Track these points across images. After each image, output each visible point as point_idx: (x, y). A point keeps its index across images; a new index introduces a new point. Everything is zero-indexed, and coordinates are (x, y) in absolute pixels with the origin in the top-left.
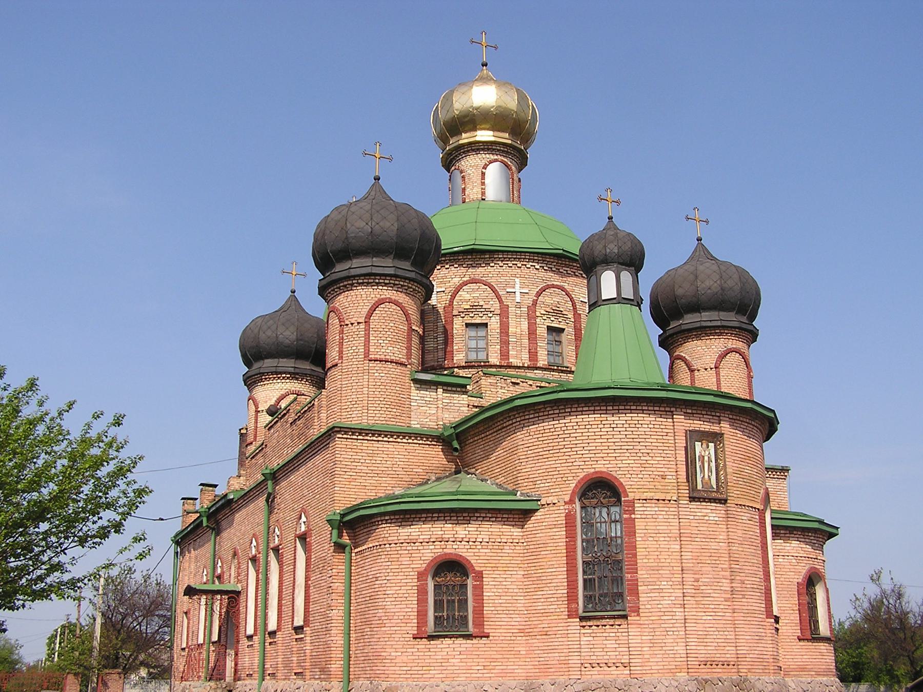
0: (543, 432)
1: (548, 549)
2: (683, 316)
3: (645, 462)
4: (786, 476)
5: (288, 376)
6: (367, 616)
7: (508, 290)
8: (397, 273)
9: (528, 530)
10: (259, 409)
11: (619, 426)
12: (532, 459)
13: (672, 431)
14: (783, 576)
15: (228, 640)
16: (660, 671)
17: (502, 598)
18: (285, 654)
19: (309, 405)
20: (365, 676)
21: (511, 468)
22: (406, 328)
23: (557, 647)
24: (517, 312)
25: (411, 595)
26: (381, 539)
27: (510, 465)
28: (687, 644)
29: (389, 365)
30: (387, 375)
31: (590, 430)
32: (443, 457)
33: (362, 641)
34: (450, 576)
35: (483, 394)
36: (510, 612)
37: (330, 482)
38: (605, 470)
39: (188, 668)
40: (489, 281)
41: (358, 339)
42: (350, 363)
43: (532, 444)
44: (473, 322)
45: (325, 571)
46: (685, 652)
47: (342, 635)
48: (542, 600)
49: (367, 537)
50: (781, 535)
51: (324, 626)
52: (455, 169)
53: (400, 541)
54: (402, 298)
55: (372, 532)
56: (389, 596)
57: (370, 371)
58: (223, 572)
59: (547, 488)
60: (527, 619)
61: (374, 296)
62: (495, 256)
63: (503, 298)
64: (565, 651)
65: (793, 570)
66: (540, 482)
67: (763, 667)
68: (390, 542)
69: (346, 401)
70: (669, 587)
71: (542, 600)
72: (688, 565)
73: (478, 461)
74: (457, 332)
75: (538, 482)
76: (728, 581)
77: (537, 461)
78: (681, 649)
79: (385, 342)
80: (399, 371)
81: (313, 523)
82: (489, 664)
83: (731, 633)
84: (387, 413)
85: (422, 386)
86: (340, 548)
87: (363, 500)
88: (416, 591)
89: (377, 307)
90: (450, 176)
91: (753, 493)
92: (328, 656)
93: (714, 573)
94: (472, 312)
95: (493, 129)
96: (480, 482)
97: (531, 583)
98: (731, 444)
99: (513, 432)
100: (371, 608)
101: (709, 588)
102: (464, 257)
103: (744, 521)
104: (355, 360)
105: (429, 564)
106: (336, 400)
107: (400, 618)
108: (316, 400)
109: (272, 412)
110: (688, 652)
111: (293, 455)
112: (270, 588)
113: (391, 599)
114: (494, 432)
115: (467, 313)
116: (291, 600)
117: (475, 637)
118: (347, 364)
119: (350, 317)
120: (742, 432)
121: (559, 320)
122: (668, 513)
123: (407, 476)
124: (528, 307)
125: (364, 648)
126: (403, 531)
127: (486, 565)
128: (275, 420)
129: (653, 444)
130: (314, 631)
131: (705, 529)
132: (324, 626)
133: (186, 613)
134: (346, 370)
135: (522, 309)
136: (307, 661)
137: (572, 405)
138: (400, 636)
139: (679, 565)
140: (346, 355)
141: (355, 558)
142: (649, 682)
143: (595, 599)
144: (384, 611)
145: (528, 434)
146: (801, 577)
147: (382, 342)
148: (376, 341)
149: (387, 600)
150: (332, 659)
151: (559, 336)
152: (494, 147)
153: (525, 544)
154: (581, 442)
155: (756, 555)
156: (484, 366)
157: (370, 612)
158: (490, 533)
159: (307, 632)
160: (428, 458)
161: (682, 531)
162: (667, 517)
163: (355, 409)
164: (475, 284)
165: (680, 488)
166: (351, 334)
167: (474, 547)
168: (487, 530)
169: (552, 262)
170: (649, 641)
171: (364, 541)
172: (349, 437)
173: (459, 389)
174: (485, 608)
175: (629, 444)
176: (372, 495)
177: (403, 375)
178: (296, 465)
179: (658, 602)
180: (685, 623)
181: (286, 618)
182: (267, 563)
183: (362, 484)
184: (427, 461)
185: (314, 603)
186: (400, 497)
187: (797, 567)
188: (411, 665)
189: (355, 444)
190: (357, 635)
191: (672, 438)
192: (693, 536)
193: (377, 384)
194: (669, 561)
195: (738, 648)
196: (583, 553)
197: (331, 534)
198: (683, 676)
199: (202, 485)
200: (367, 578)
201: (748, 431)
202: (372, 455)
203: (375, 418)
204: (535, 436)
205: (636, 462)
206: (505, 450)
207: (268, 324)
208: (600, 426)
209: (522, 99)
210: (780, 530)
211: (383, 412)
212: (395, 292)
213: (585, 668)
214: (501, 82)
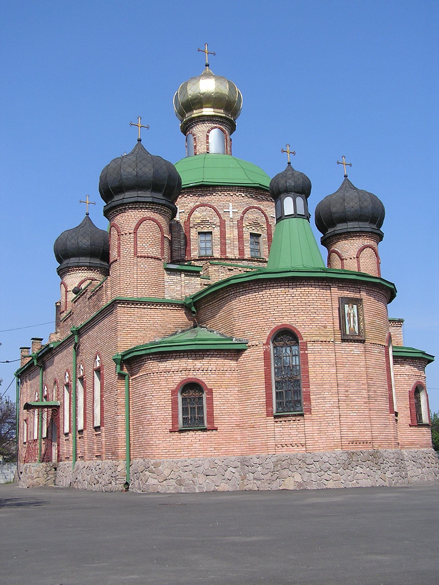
0: (248, 300)
3: (313, 318)
4: (401, 325)
6: (140, 419)
7: (225, 210)
8: (153, 201)
9: (240, 362)
10: (68, 290)
12: (242, 317)
16: (325, 448)
17: (225, 405)
19: (100, 287)
22: (160, 236)
23: (260, 435)
25: (167, 405)
26: (148, 370)
27: (228, 321)
28: (341, 431)
30: (149, 266)
31: (278, 298)
32: (186, 317)
33: (138, 434)
34: (191, 392)
36: (230, 414)
38: (288, 323)
41: (129, 243)
42: (125, 259)
43: (242, 308)
44: (203, 231)
45: (113, 391)
47: (125, 431)
49: (139, 369)
50: (399, 362)
51: (113, 426)
52: (190, 133)
53: (160, 371)
54: (157, 216)
55: (142, 366)
56: (154, 406)
57: (138, 264)
58: (48, 394)
59: (252, 335)
60: (241, 418)
62: (216, 189)
65: (407, 383)
66: (247, 332)
67: (388, 444)
68: (154, 372)
69: (123, 283)
72: (341, 382)
75: (246, 332)
76: (366, 391)
77: (245, 319)
78: (337, 434)
79: (147, 245)
80: (156, 263)
82: (218, 447)
83: (368, 423)
84: (149, 290)
86: (122, 376)
88: (171, 402)
89: (142, 223)
92: (116, 444)
93: (357, 386)
94: (202, 225)
95: (213, 107)
96: (209, 333)
97: (243, 395)
99: (230, 301)
100: (143, 414)
101: (354, 395)
102: (197, 190)
103: (376, 354)
107: (161, 419)
108: (104, 283)
109: (76, 292)
111: (90, 318)
117: (209, 430)
118: (123, 260)
122: (328, 349)
126: (162, 364)
127: (215, 385)
128: (78, 297)
132: (113, 426)
133: (25, 420)
134: (123, 264)
135: (234, 222)
137: (266, 282)
138: (161, 431)
142: (318, 455)
143: (283, 404)
145: (239, 302)
146: (411, 388)
147: (145, 245)
149: (152, 408)
150: (119, 446)
153: (239, 371)
155: (383, 374)
156: (210, 259)
157: (142, 416)
158: (217, 365)
160: (176, 318)
161: (337, 361)
162: (328, 352)
163: (129, 288)
164: (203, 207)
167: (207, 374)
168: (214, 362)
169: (253, 192)
170: (317, 430)
173: (195, 274)
175: (303, 306)
176: (141, 342)
178: (93, 325)
179: (323, 405)
180: (340, 418)
182: (76, 387)
184: (176, 320)
187: (409, 381)
190: (134, 431)
191: (330, 302)
192: (344, 363)
193: (143, 272)
194: (329, 379)
198: (339, 450)
200: (140, 395)
202: (141, 317)
203: (142, 294)
204: (243, 303)
206: (225, 312)
208: (284, 296)
211: (147, 290)
212: (153, 213)
214: (218, 77)
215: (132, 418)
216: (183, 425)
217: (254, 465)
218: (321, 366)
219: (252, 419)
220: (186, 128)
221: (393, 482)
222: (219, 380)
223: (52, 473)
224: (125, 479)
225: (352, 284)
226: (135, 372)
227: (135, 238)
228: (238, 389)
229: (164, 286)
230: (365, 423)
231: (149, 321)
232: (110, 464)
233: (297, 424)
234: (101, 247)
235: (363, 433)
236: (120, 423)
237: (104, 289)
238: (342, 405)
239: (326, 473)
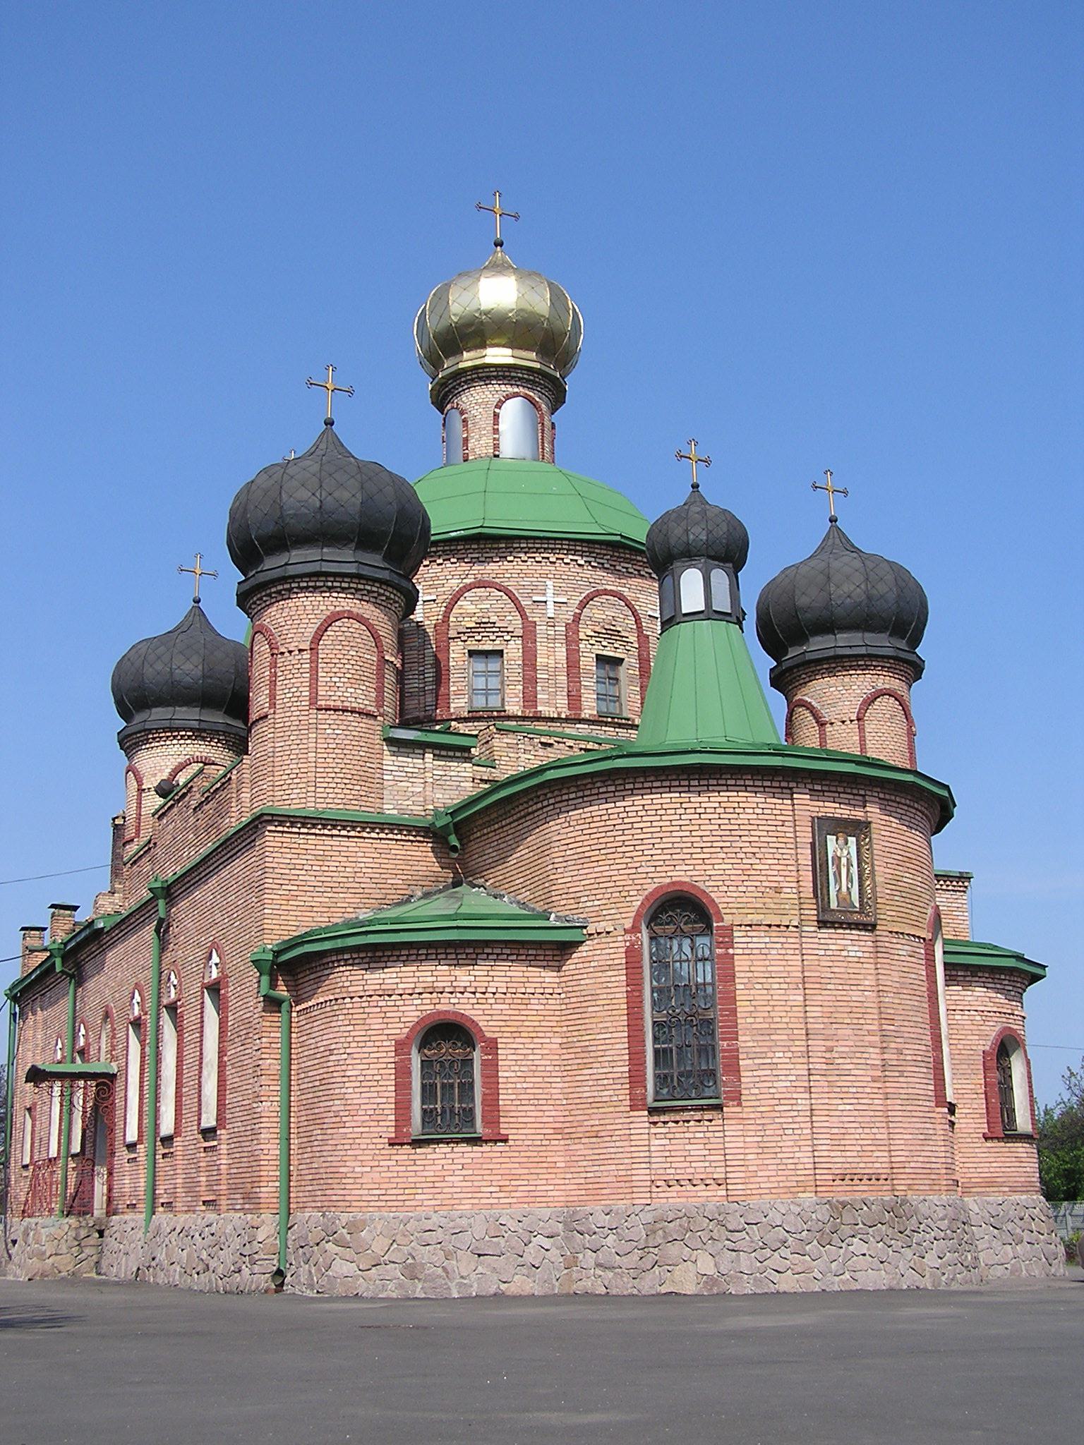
0: (590, 820)
1: (598, 1003)
3: (749, 867)
6: (316, 1111)
7: (535, 598)
9: (567, 973)
10: (144, 787)
12: (573, 862)
16: (773, 1191)
17: (528, 1080)
19: (223, 780)
21: (541, 877)
23: (613, 1156)
25: (384, 1077)
26: (338, 990)
27: (539, 873)
30: (345, 732)
31: (664, 818)
33: (309, 1150)
34: (445, 1047)
36: (541, 1102)
38: (687, 879)
41: (299, 675)
42: (288, 714)
43: (573, 840)
44: (481, 648)
45: (250, 1040)
46: (811, 1160)
47: (278, 1141)
48: (591, 1083)
49: (315, 986)
51: (249, 1128)
52: (453, 408)
53: (367, 993)
55: (323, 978)
56: (351, 1079)
57: (319, 726)
58: (88, 1044)
59: (597, 908)
60: (567, 1113)
61: (324, 608)
62: (515, 545)
64: (626, 1161)
65: (977, 1033)
66: (586, 899)
68: (352, 995)
69: (282, 773)
70: (788, 1060)
71: (591, 1083)
72: (816, 1026)
74: (454, 664)
75: (583, 899)
76: (877, 1050)
77: (580, 867)
78: (805, 1157)
79: (342, 680)
80: (364, 725)
82: (508, 1183)
83: (882, 1131)
84: (345, 791)
85: (401, 750)
86: (273, 1004)
87: (309, 929)
88: (393, 1071)
89: (330, 625)
90: (444, 419)
92: (256, 1174)
93: (856, 1038)
97: (573, 1056)
100: (323, 1099)
101: (848, 1061)
103: (903, 958)
105: (412, 1029)
106: (265, 772)
107: (369, 1112)
108: (235, 772)
109: (164, 790)
110: (817, 1160)
111: (198, 859)
112: (163, 1067)
114: (514, 821)
117: (486, 1142)
118: (283, 715)
119: (288, 641)
120: (900, 819)
122: (785, 946)
126: (373, 976)
127: (503, 1029)
128: (169, 804)
132: (249, 1128)
133: (29, 1110)
134: (282, 725)
135: (557, 628)
136: (222, 1182)
138: (369, 1141)
142: (757, 1207)
143: (672, 1080)
144: (343, 1102)
145: (567, 824)
146: (989, 1043)
147: (337, 680)
149: (347, 1085)
150: (262, 1179)
152: (513, 374)
153: (563, 996)
155: (921, 1010)
157: (321, 1104)
159: (222, 1137)
160: (411, 863)
162: (783, 952)
163: (295, 786)
164: (483, 589)
165: (804, 906)
166: (288, 668)
167: (484, 1001)
168: (503, 974)
170: (756, 1145)
173: (458, 754)
174: (501, 1097)
175: (724, 839)
176: (322, 920)
178: (203, 874)
182: (158, 1029)
184: (409, 868)
187: (983, 1028)
190: (300, 1140)
191: (792, 830)
192: (823, 981)
193: (330, 746)
194: (787, 1020)
197: (259, 982)
198: (808, 1197)
199: (53, 906)
200: (316, 1051)
201: (908, 819)
202: (322, 858)
203: (327, 801)
204: (577, 828)
205: (735, 866)
206: (531, 849)
208: (679, 811)
210: (957, 971)
211: (340, 791)
214: (524, 272)
215: (296, 1109)
216: (423, 1124)
217: (597, 1230)
219: (594, 1117)
220: (444, 396)
221: (944, 1278)
222: (513, 1018)
223: (92, 1243)
224: (275, 1262)
227: (314, 661)
228: (560, 1041)
230: (874, 1131)
232: (238, 1223)
233: (705, 1129)
235: (870, 1154)
236: (267, 1120)
237: (234, 786)
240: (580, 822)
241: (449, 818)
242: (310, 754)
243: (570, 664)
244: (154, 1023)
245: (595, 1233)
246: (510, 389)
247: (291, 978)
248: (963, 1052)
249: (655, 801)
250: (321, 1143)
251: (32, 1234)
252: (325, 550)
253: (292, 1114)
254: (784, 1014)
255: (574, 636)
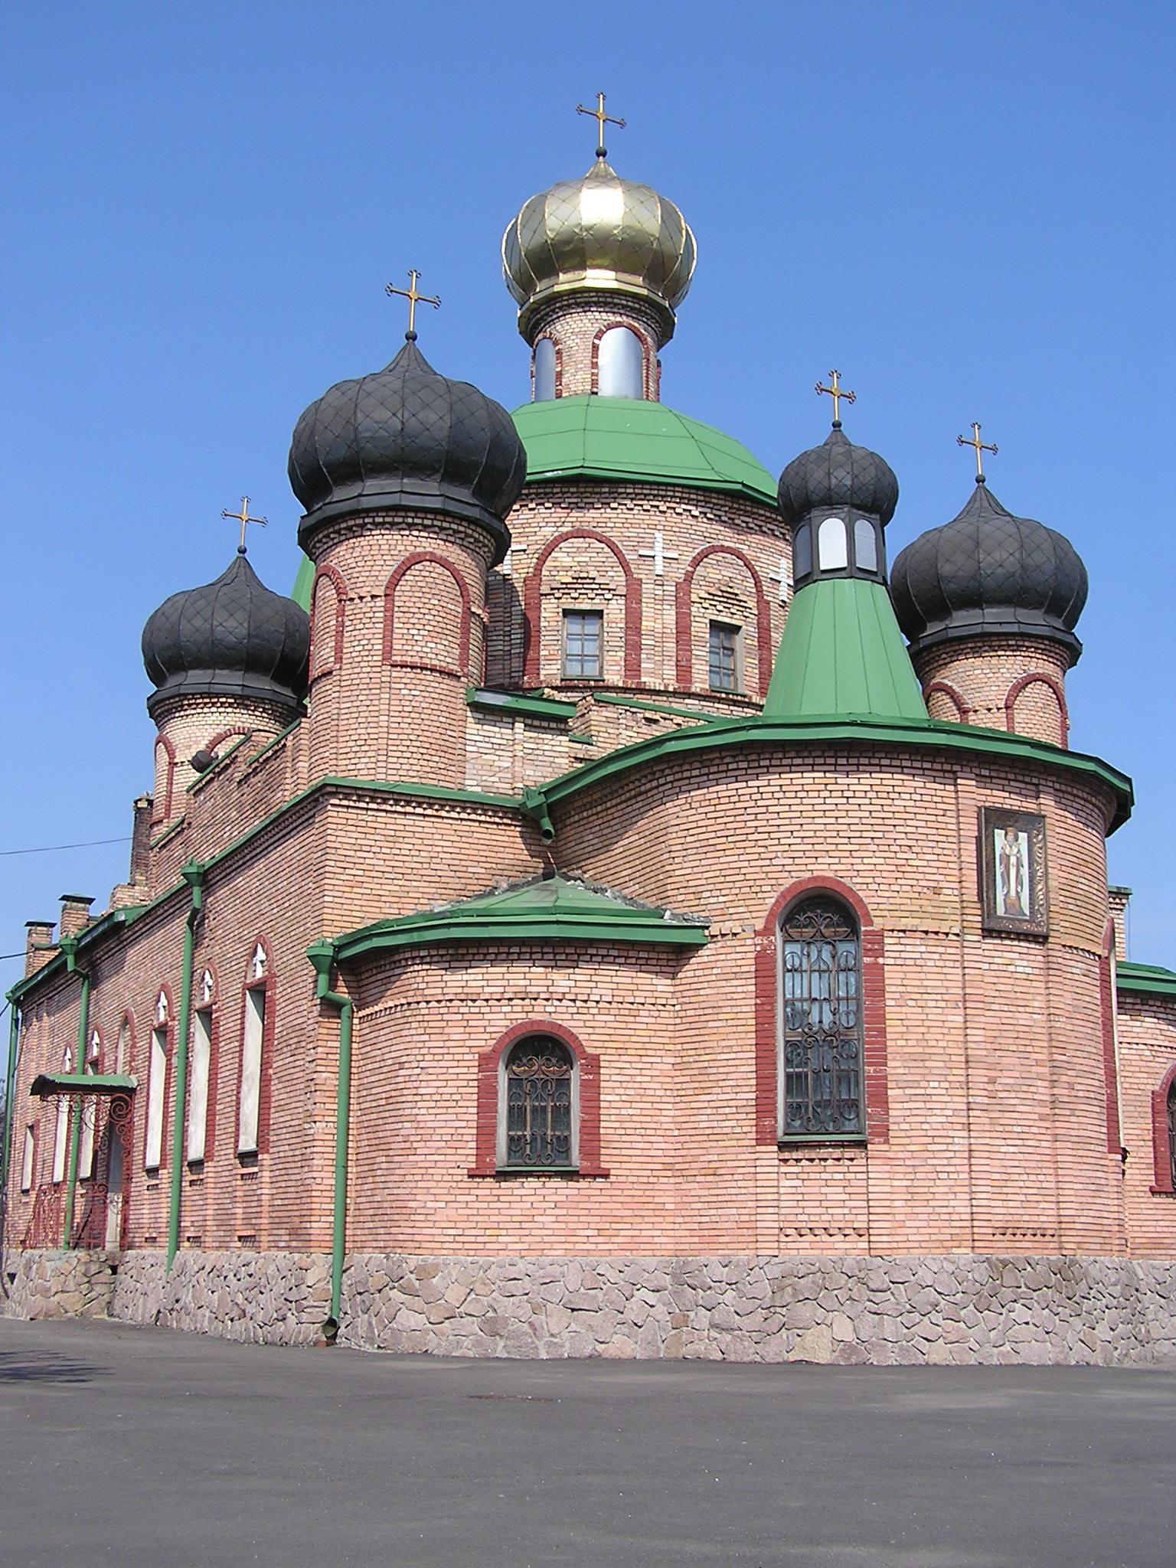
0: (716, 801)
1: (721, 1017)
2: (951, 614)
4: (1123, 905)
5: (229, 700)
6: (381, 1134)
7: (642, 552)
8: (447, 508)
9: (683, 982)
10: (176, 760)
11: (858, 794)
12: (694, 851)
13: (953, 807)
14: (1127, 1080)
15: (111, 1176)
16: (924, 1245)
17: (634, 1105)
18: (220, 1201)
19: (276, 748)
20: (375, 1244)
21: (654, 867)
22: (460, 610)
23: (734, 1198)
24: (657, 592)
25: (465, 1097)
26: (411, 993)
27: (651, 863)
28: (974, 1196)
29: (429, 676)
30: (424, 694)
31: (805, 801)
32: (523, 847)
33: (370, 1180)
34: (538, 1063)
35: (594, 738)
36: (649, 1132)
37: (314, 886)
38: (831, 874)
39: (37, 1225)
40: (608, 534)
41: (371, 625)
42: (356, 670)
43: (694, 825)
44: (577, 607)
45: (301, 1050)
46: (968, 1210)
47: (333, 1169)
48: (709, 1111)
49: (383, 988)
51: (297, 1152)
52: (545, 338)
53: (447, 997)
55: (393, 979)
56: (425, 1098)
57: (393, 686)
58: (102, 1054)
59: (722, 906)
60: (679, 1146)
61: (403, 548)
62: (620, 490)
63: (632, 566)
64: (750, 1204)
65: (1146, 1070)
66: (708, 894)
67: (1101, 1240)
68: (429, 999)
69: (347, 738)
70: (944, 1092)
71: (709, 1111)
72: (978, 1052)
73: (587, 856)
74: (546, 624)
75: (705, 895)
76: (1046, 1084)
77: (703, 856)
78: (961, 1206)
79: (422, 632)
80: (445, 687)
81: (279, 962)
82: (607, 1226)
83: (1049, 1178)
84: (422, 762)
85: (487, 717)
86: (331, 1008)
87: (374, 922)
88: (476, 1090)
89: (409, 568)
90: (534, 351)
91: (1091, 926)
92: (306, 1207)
93: (1022, 1068)
94: (576, 589)
96: (592, 894)
97: (688, 1079)
98: (1057, 836)
99: (659, 802)
100: (390, 1120)
101: (1013, 1095)
102: (564, 490)
103: (1076, 977)
104: (366, 664)
105: (500, 1040)
106: (328, 737)
107: (445, 1138)
108: (290, 738)
109: (200, 763)
110: (975, 1210)
111: (242, 839)
112: (193, 1081)
113: (427, 1104)
114: (622, 802)
115: (566, 591)
116: (234, 1103)
117: (584, 1176)
118: (350, 671)
119: (358, 585)
120: (1076, 815)
121: (732, 610)
122: (945, 957)
123: (457, 880)
124: (677, 583)
125: (374, 1192)
126: (454, 977)
127: (607, 1044)
128: (208, 777)
129: (920, 830)
130: (277, 1161)
131: (1009, 988)
132: (297, 1152)
133: (31, 1128)
134: (349, 682)
135: (665, 588)
136: (263, 1215)
137: (772, 753)
138: (444, 1171)
139: (962, 1052)
140: (349, 655)
141: (358, 1028)
142: (904, 1263)
143: (807, 1111)
144: (415, 1125)
145: (688, 806)
146: (1159, 1082)
147: (416, 632)
148: (406, 631)
149: (419, 1104)
150: (314, 1212)
151: (730, 639)
152: (615, 301)
153: (678, 1008)
154: (787, 821)
155: (1094, 1038)
156: (594, 687)
157: (387, 1127)
158: (614, 986)
159: (265, 1162)
160: (496, 849)
161: (968, 991)
162: (941, 964)
163: (363, 754)
165: (967, 911)
166: (358, 616)
167: (586, 1011)
168: (609, 979)
169: (722, 506)
170: (904, 1190)
171: (376, 997)
172: (352, 804)
174: (602, 1124)
175: (876, 828)
176: (391, 912)
177: (453, 694)
178: (248, 857)
179: (923, 1119)
180: (970, 1158)
181: (224, 1137)
182: (188, 1038)
183: (374, 892)
185: (279, 1109)
186: (449, 914)
187: (1152, 1064)
188: (463, 1225)
189: (363, 817)
190: (360, 1169)
191: (954, 821)
192: (987, 1000)
193: (406, 709)
194: (944, 1044)
195: (1062, 1205)
196: (785, 1025)
197: (316, 981)
198: (963, 1254)
199: (64, 898)
200: (382, 1064)
201: (1084, 815)
202: (393, 839)
203: (401, 773)
204: (700, 810)
206: (641, 835)
207: (196, 606)
208: (822, 794)
209: (669, 217)
211: (416, 762)
212: (442, 543)
213: (787, 1236)
214: (631, 181)
215: (355, 1132)
216: (509, 1155)
217: (713, 1284)
218: (920, 1003)
219: (711, 1151)
221: (1116, 1354)
222: (618, 1032)
224: (327, 1310)
225: (1017, 771)
226: (371, 999)
227: (389, 610)
228: (672, 1060)
229: (464, 753)
230: (1041, 1178)
231: (417, 853)
232: (283, 1264)
234: (278, 645)
235: (1035, 1205)
236: (321, 1143)
237: (289, 753)
238: (977, 1120)
239: (926, 1319)
240: (703, 804)
241: (542, 798)
242: (381, 718)
243: (679, 630)
244: (184, 1029)
245: (710, 1288)
246: (612, 318)
247: (353, 978)
248: (1129, 1091)
249: (794, 782)
250: (385, 1173)
251: (35, 1267)
252: (405, 481)
253: (351, 1138)
254: (940, 1037)
255: (686, 597)
